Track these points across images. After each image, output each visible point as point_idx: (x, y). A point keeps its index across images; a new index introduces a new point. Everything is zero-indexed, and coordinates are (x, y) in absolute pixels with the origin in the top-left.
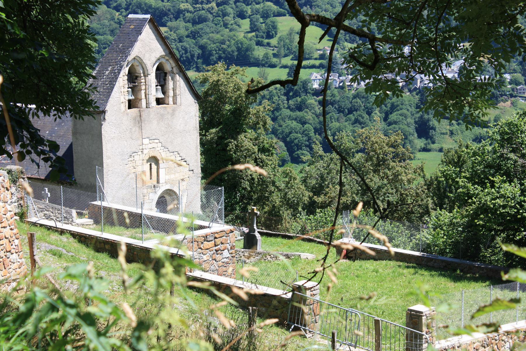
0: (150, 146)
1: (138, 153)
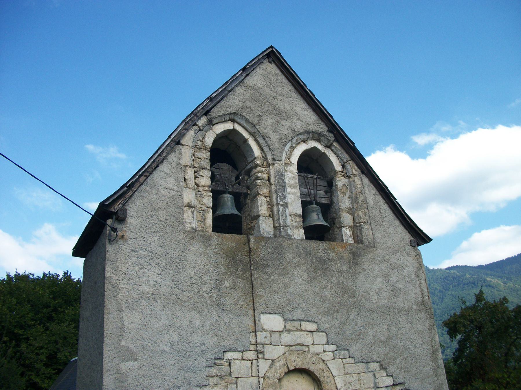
0: (287, 338)
1: (246, 355)
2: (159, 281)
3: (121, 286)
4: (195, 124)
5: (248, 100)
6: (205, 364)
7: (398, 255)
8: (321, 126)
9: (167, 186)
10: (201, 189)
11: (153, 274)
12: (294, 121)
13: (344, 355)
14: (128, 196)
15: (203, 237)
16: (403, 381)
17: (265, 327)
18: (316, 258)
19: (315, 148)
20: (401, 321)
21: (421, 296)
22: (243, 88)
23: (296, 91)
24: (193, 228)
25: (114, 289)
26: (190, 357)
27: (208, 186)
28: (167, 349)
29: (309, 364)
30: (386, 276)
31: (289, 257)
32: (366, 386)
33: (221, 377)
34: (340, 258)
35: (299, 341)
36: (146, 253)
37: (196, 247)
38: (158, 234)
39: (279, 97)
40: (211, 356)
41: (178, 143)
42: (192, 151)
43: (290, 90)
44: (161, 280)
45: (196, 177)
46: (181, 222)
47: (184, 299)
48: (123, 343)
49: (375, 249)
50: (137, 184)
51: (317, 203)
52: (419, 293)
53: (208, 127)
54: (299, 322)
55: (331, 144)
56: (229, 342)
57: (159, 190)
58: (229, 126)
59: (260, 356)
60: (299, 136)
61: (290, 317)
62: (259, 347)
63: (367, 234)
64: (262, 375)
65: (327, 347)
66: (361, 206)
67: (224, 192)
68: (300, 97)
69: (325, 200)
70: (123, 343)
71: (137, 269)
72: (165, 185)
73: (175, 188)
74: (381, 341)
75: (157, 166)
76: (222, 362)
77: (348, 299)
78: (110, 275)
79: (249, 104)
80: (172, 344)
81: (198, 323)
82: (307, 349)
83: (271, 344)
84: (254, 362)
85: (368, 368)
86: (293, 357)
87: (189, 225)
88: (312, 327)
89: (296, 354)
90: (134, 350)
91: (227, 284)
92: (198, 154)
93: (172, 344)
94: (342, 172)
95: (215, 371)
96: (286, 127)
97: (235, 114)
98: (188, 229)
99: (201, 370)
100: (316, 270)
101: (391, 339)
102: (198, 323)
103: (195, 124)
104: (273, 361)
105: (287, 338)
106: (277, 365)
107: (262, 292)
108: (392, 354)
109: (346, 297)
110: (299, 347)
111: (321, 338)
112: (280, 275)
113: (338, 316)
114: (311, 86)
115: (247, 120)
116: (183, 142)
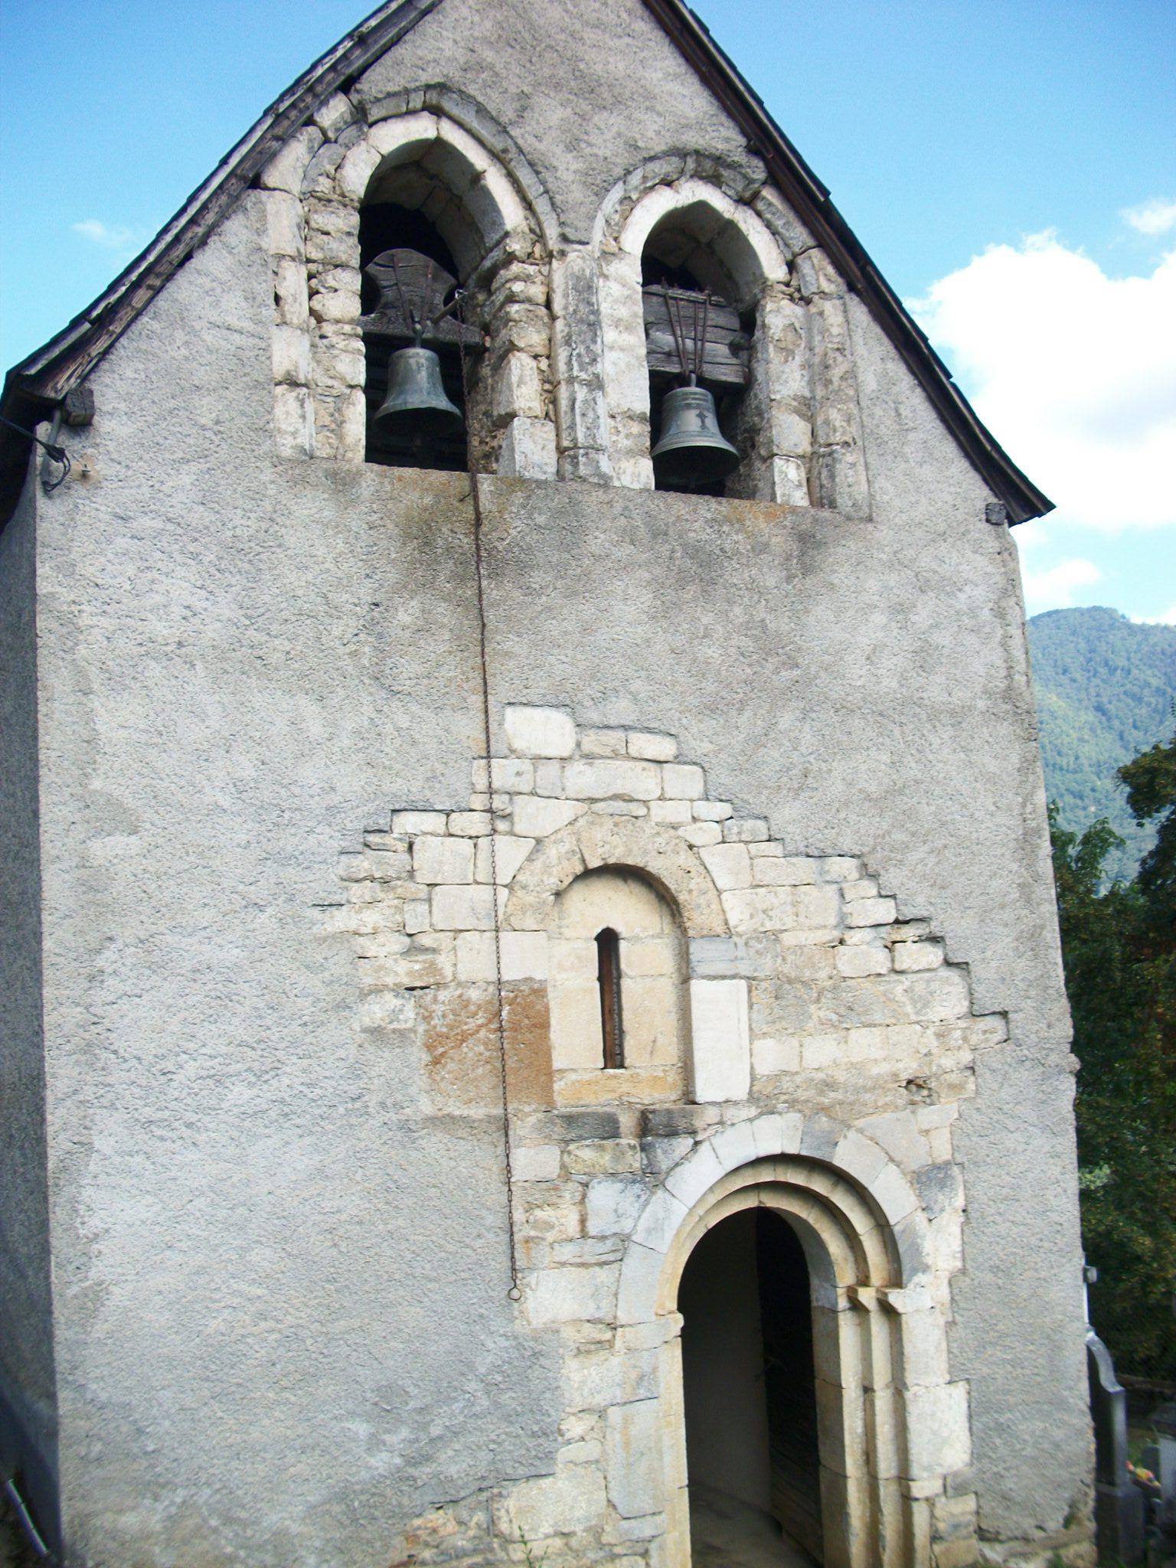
0: (583, 779)
1: (459, 822)
2: (199, 605)
4: (310, 122)
6: (336, 845)
9: (218, 321)
10: (328, 329)
12: (637, 115)
13: (753, 831)
14: (96, 349)
15: (333, 475)
16: (925, 914)
20: (936, 742)
21: (1003, 673)
23: (646, 14)
25: (64, 630)
27: (351, 322)
28: (225, 801)
29: (645, 852)
30: (901, 610)
31: (598, 541)
33: (385, 882)
36: (158, 524)
38: (194, 467)
39: (590, 35)
41: (256, 183)
42: (300, 209)
43: (629, 12)
44: (206, 604)
45: (313, 293)
46: (266, 431)
47: (276, 658)
48: (96, 784)
49: (870, 527)
50: (125, 314)
51: (702, 382)
52: (1000, 663)
56: (412, 787)
58: (423, 128)
59: (502, 826)
60: (650, 166)
61: (594, 716)
62: (499, 802)
63: (850, 480)
64: (504, 878)
65: (704, 809)
66: (837, 392)
67: (409, 343)
69: (728, 374)
70: (96, 784)
71: (131, 570)
73: (248, 325)
74: (868, 798)
75: (188, 257)
76: (388, 840)
77: (777, 671)
78: (50, 589)
79: (489, 55)
80: (239, 788)
81: (315, 729)
82: (642, 811)
83: (533, 793)
86: (600, 833)
87: (289, 441)
88: (664, 748)
89: (609, 823)
90: (129, 802)
92: (320, 220)
93: (239, 788)
94: (787, 285)
95: (366, 864)
96: (608, 136)
97: (442, 88)
98: (287, 452)
99: (324, 862)
100: (682, 581)
101: (901, 792)
102: (315, 729)
103: (310, 122)
104: (539, 841)
105: (583, 779)
106: (552, 852)
107: (511, 643)
108: (899, 836)
109: (770, 666)
111: (686, 781)
112: (571, 594)
115: (481, 110)
116: (270, 178)
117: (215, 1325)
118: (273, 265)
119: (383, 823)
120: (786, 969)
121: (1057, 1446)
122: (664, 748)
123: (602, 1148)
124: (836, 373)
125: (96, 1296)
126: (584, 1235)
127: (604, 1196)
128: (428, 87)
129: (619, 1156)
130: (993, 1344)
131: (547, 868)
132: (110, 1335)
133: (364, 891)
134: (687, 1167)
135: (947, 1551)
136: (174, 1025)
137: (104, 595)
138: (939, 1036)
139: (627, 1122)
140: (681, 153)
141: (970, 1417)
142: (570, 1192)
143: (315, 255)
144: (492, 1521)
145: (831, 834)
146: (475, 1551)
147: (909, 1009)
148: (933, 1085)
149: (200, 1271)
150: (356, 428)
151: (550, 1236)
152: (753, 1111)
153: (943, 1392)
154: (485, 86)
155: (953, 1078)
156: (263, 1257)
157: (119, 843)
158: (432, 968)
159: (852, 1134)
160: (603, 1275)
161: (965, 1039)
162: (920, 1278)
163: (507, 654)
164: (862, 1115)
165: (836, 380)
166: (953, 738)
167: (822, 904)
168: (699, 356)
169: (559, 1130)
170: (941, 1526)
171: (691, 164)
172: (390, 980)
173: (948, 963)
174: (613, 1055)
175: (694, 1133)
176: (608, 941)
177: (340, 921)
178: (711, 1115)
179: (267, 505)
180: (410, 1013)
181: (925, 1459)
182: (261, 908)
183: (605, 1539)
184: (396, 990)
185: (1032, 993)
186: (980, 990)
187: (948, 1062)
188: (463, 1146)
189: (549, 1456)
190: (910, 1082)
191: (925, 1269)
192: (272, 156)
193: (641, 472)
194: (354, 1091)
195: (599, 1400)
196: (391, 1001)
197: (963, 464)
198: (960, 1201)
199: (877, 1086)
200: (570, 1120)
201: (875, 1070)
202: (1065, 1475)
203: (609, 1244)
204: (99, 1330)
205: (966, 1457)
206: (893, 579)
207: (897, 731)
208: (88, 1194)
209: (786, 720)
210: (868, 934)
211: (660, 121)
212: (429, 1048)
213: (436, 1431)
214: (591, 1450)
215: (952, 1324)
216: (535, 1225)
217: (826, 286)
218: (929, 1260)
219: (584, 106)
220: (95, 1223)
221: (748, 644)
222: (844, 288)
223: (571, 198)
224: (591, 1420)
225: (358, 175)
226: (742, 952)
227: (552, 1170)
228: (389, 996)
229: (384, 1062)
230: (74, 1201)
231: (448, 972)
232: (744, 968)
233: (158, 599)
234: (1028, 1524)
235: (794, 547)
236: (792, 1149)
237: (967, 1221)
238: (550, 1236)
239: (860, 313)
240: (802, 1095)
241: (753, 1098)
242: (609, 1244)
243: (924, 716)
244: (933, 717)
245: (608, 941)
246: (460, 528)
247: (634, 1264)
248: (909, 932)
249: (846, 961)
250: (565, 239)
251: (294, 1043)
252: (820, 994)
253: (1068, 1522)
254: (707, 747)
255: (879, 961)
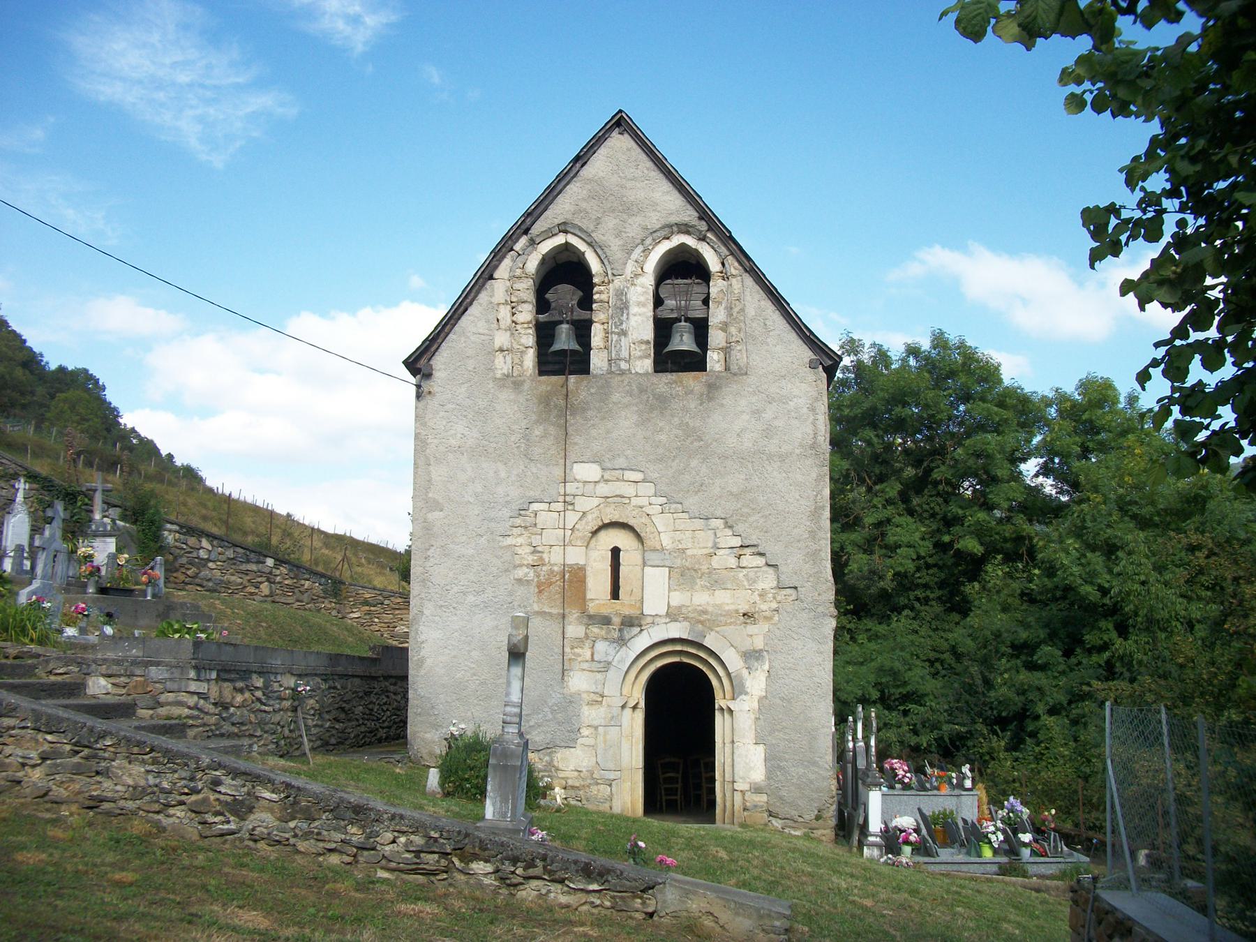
0: (603, 489)
1: (554, 506)
2: (466, 433)
3: (429, 441)
4: (512, 249)
5: (584, 199)
6: (508, 515)
7: (783, 382)
8: (689, 213)
10: (518, 327)
11: (460, 428)
12: (648, 214)
13: (675, 509)
14: (433, 349)
15: (514, 383)
17: (577, 477)
18: (654, 395)
19: (683, 245)
20: (770, 469)
21: (812, 436)
22: (578, 184)
23: (656, 168)
24: (504, 375)
26: (493, 507)
27: (528, 323)
29: (628, 517)
30: (757, 413)
31: (616, 397)
32: (701, 545)
33: (526, 527)
34: (689, 392)
35: (618, 493)
36: (454, 406)
37: (506, 395)
38: (466, 385)
39: (629, 184)
40: (515, 506)
41: (491, 278)
42: (508, 284)
43: (648, 169)
45: (513, 314)
46: (491, 369)
47: (490, 450)
48: (430, 495)
49: (745, 377)
50: (442, 335)
51: (687, 319)
52: (812, 432)
53: (530, 248)
54: (621, 472)
55: (705, 236)
56: (533, 494)
57: (468, 337)
58: (560, 240)
59: (570, 507)
60: (655, 235)
61: (609, 465)
62: (568, 499)
65: (653, 500)
66: (734, 319)
67: (561, 322)
68: (661, 175)
69: (699, 314)
70: (430, 495)
71: (444, 423)
72: (474, 330)
73: (486, 332)
74: (732, 494)
75: (466, 310)
76: (527, 513)
77: (692, 443)
79: (584, 205)
80: (476, 495)
81: (503, 475)
82: (627, 501)
83: (583, 495)
84: (562, 513)
85: (707, 525)
86: (609, 510)
87: (500, 372)
88: (638, 476)
89: (613, 506)
90: (441, 501)
91: (537, 433)
92: (516, 286)
93: (476, 495)
94: (722, 272)
96: (635, 226)
97: (564, 223)
98: (498, 376)
100: (652, 409)
101: (750, 491)
102: (503, 475)
103: (512, 249)
104: (584, 513)
105: (603, 489)
106: (590, 517)
107: (577, 439)
108: (746, 510)
109: (689, 441)
110: (619, 499)
111: (649, 489)
112: (603, 418)
113: (674, 464)
114: (673, 160)
115: (581, 229)
116: (495, 276)
117: (459, 675)
118: (496, 307)
119: (525, 507)
120: (687, 564)
121: (811, 782)
122: (638, 476)
123: (602, 628)
124: (736, 310)
125: (421, 662)
126: (593, 660)
127: (601, 646)
128: (559, 225)
129: (609, 632)
130: (779, 731)
131: (587, 523)
132: (426, 674)
133: (517, 531)
134: (636, 639)
135: (750, 816)
136: (451, 574)
137: (435, 432)
138: (760, 595)
139: (616, 620)
140: (671, 226)
141: (765, 760)
142: (588, 644)
143: (514, 299)
144: (552, 760)
145: (711, 509)
146: (545, 771)
147: (746, 583)
148: (756, 616)
149: (455, 657)
150: (530, 359)
151: (579, 659)
152: (668, 620)
153: (752, 747)
154: (582, 218)
155: (767, 614)
156: (475, 654)
157: (437, 514)
158: (541, 559)
159: (713, 633)
160: (599, 676)
161: (774, 598)
162: (743, 697)
163: (576, 444)
164: (718, 626)
165: (735, 314)
166: (780, 467)
167: (706, 539)
168: (687, 308)
169: (585, 620)
170: (748, 804)
171: (675, 229)
172: (525, 562)
173: (768, 565)
174: (615, 594)
175: (641, 626)
176: (616, 552)
177: (509, 541)
178: (649, 620)
179: (490, 396)
180: (531, 575)
181: (741, 774)
182: (482, 536)
183: (594, 776)
184: (527, 566)
185: (811, 579)
186: (783, 577)
187: (764, 607)
188: (548, 623)
189: (575, 740)
190: (744, 615)
191: (746, 693)
192: (496, 267)
193: (647, 364)
194: (510, 600)
195: (595, 723)
196: (526, 570)
197: (800, 342)
198: (766, 667)
199: (728, 614)
200: (590, 617)
201: (727, 608)
202: (815, 796)
203: (602, 665)
204: (422, 672)
205: (763, 778)
206: (754, 399)
207: (750, 465)
208: (421, 628)
209: (694, 463)
210: (728, 551)
211: (658, 214)
212: (538, 587)
213: (532, 723)
214: (591, 741)
215: (757, 719)
216: (574, 654)
217: (734, 272)
218: (749, 690)
219: (625, 216)
220: (423, 637)
221: (680, 433)
222: (743, 271)
223: (616, 257)
224: (592, 730)
225: (533, 263)
226: (667, 556)
227: (582, 635)
228: (524, 568)
229: (521, 591)
230: (417, 629)
231: (547, 560)
232: (667, 563)
233: (453, 432)
234: (794, 813)
235: (705, 391)
236: (685, 636)
237: (769, 676)
238: (579, 659)
239: (749, 281)
240: (691, 615)
241: (668, 614)
242: (602, 665)
243: (765, 458)
244: (770, 457)
245: (616, 552)
246: (560, 397)
247: (611, 674)
248: (747, 551)
249: (715, 562)
250: (614, 275)
251: (490, 582)
252: (703, 574)
253: (818, 818)
254: (656, 475)
255: (733, 562)
